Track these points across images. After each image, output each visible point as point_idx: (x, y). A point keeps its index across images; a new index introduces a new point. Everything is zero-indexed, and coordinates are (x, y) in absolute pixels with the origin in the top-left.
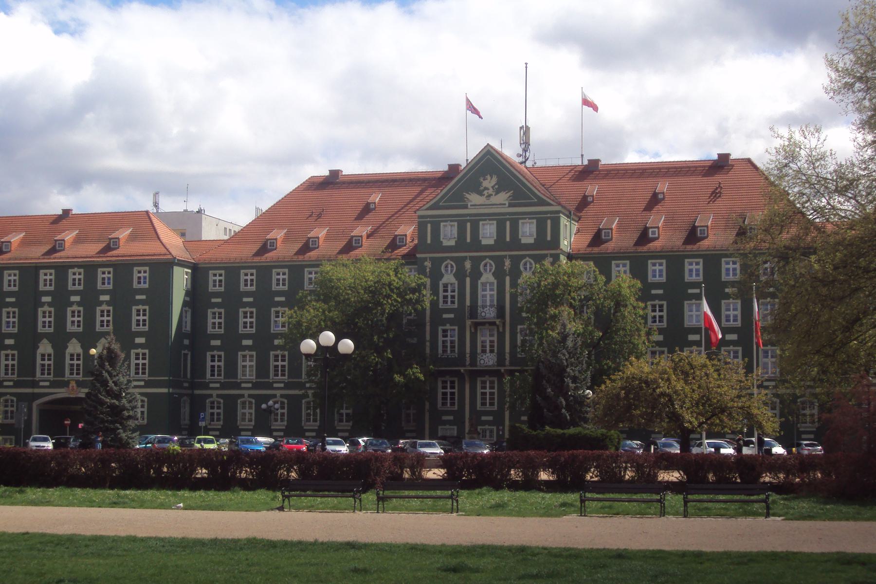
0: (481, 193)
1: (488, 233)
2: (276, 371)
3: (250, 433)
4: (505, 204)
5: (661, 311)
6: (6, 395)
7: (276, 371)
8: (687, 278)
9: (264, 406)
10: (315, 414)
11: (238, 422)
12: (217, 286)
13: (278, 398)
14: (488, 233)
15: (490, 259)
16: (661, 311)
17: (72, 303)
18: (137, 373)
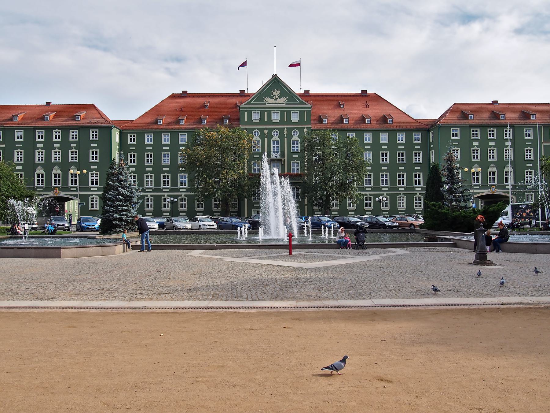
0: (272, 98)
1: (276, 118)
2: (383, 182)
3: (202, 214)
4: (284, 103)
5: (151, 157)
6: (93, 195)
7: (383, 182)
8: (163, 142)
9: (377, 199)
10: (202, 204)
11: (162, 208)
12: (166, 141)
13: (385, 196)
14: (276, 118)
15: (277, 130)
16: (151, 157)
17: (72, 148)
18: (72, 184)
